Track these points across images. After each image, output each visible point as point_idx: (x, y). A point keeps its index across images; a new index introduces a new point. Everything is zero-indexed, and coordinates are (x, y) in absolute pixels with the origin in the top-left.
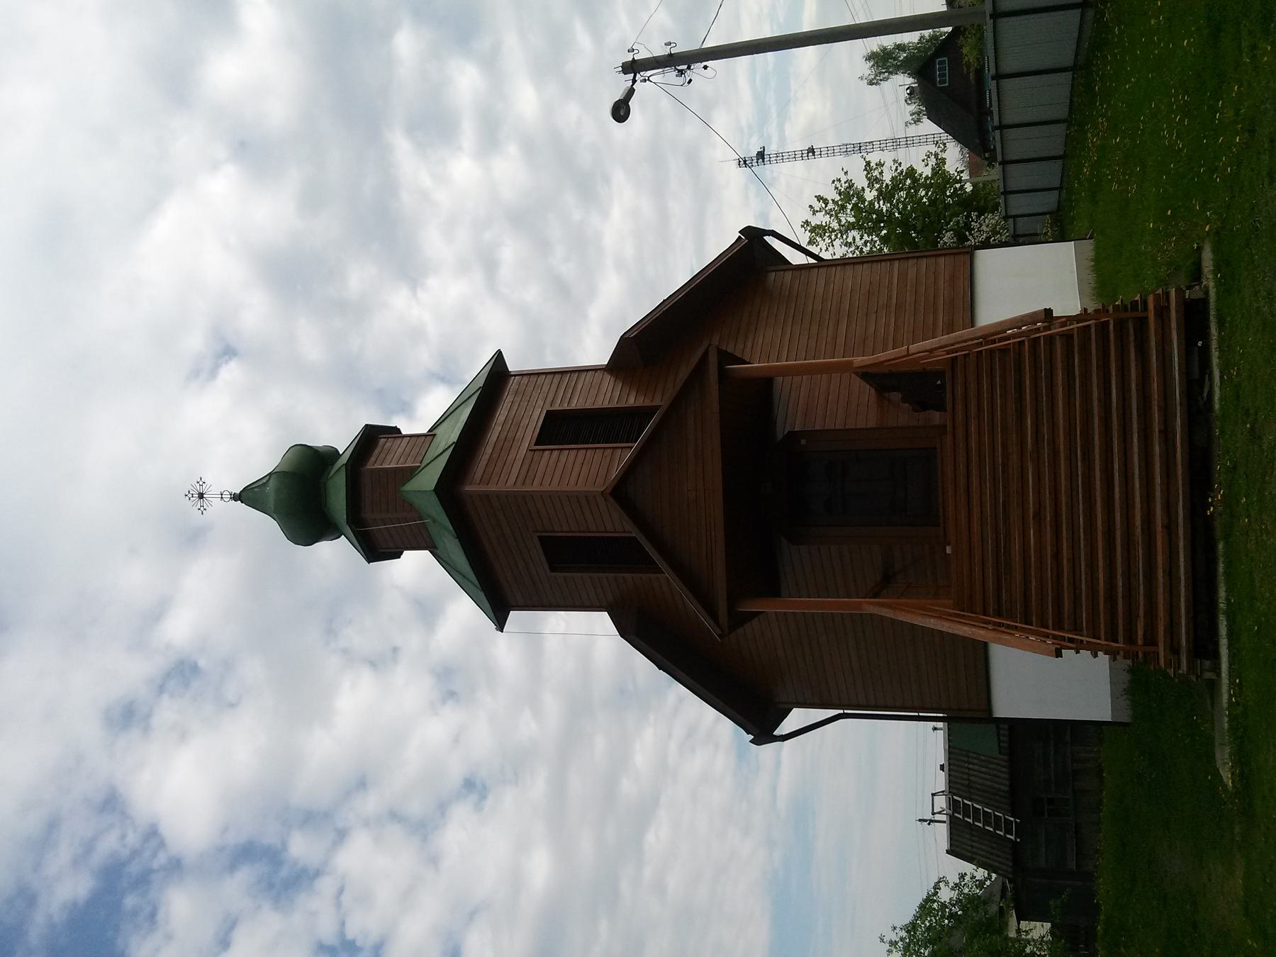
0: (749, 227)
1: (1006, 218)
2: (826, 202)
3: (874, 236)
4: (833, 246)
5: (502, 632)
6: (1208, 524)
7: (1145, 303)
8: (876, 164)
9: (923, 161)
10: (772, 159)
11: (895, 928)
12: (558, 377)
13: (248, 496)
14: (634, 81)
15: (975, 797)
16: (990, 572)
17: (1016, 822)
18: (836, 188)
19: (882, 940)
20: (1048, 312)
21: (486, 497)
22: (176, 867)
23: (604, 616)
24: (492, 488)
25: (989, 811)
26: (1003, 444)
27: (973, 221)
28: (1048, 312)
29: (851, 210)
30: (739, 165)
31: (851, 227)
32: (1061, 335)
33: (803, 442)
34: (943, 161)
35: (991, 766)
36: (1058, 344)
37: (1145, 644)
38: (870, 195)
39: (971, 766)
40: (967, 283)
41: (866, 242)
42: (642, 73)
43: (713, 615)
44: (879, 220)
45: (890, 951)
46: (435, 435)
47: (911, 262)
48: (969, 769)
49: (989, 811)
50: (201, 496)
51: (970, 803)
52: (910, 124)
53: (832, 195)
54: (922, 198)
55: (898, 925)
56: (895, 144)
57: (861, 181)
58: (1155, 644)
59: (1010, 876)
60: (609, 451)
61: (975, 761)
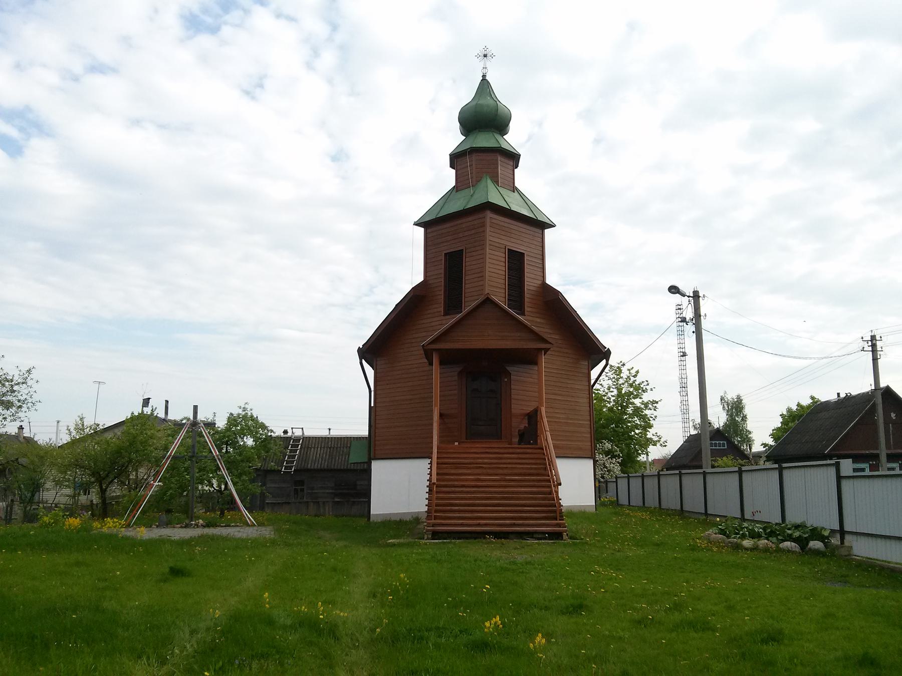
0: (610, 353)
1: (616, 478)
2: (635, 376)
3: (613, 403)
4: (609, 379)
5: (414, 225)
7: (563, 520)
8: (655, 407)
9: (656, 433)
10: (680, 327)
12: (541, 257)
13: (484, 86)
14: (689, 297)
15: (302, 451)
16: (452, 461)
17: (291, 472)
18: (643, 382)
19: (246, 403)
20: (560, 484)
21: (483, 225)
23: (422, 279)
24: (488, 229)
25: (296, 458)
26: (507, 467)
27: (616, 459)
28: (560, 484)
29: (629, 390)
30: (678, 305)
31: (619, 390)
32: (551, 491)
33: (506, 380)
34: (655, 445)
35: (320, 459)
36: (548, 489)
37: (435, 516)
38: (637, 402)
39: (319, 449)
40: (398, 457)
41: (610, 398)
42: (692, 301)
43: (433, 342)
44: (622, 406)
45: (240, 407)
46: (514, 192)
47: (589, 430)
48: (318, 448)
49: (296, 458)
50: (485, 56)
51: (299, 448)
52: (694, 422)
53: (639, 380)
54: (634, 432)
56: (685, 411)
57: (646, 397)
59: (262, 468)
60: (504, 287)
61: (322, 451)
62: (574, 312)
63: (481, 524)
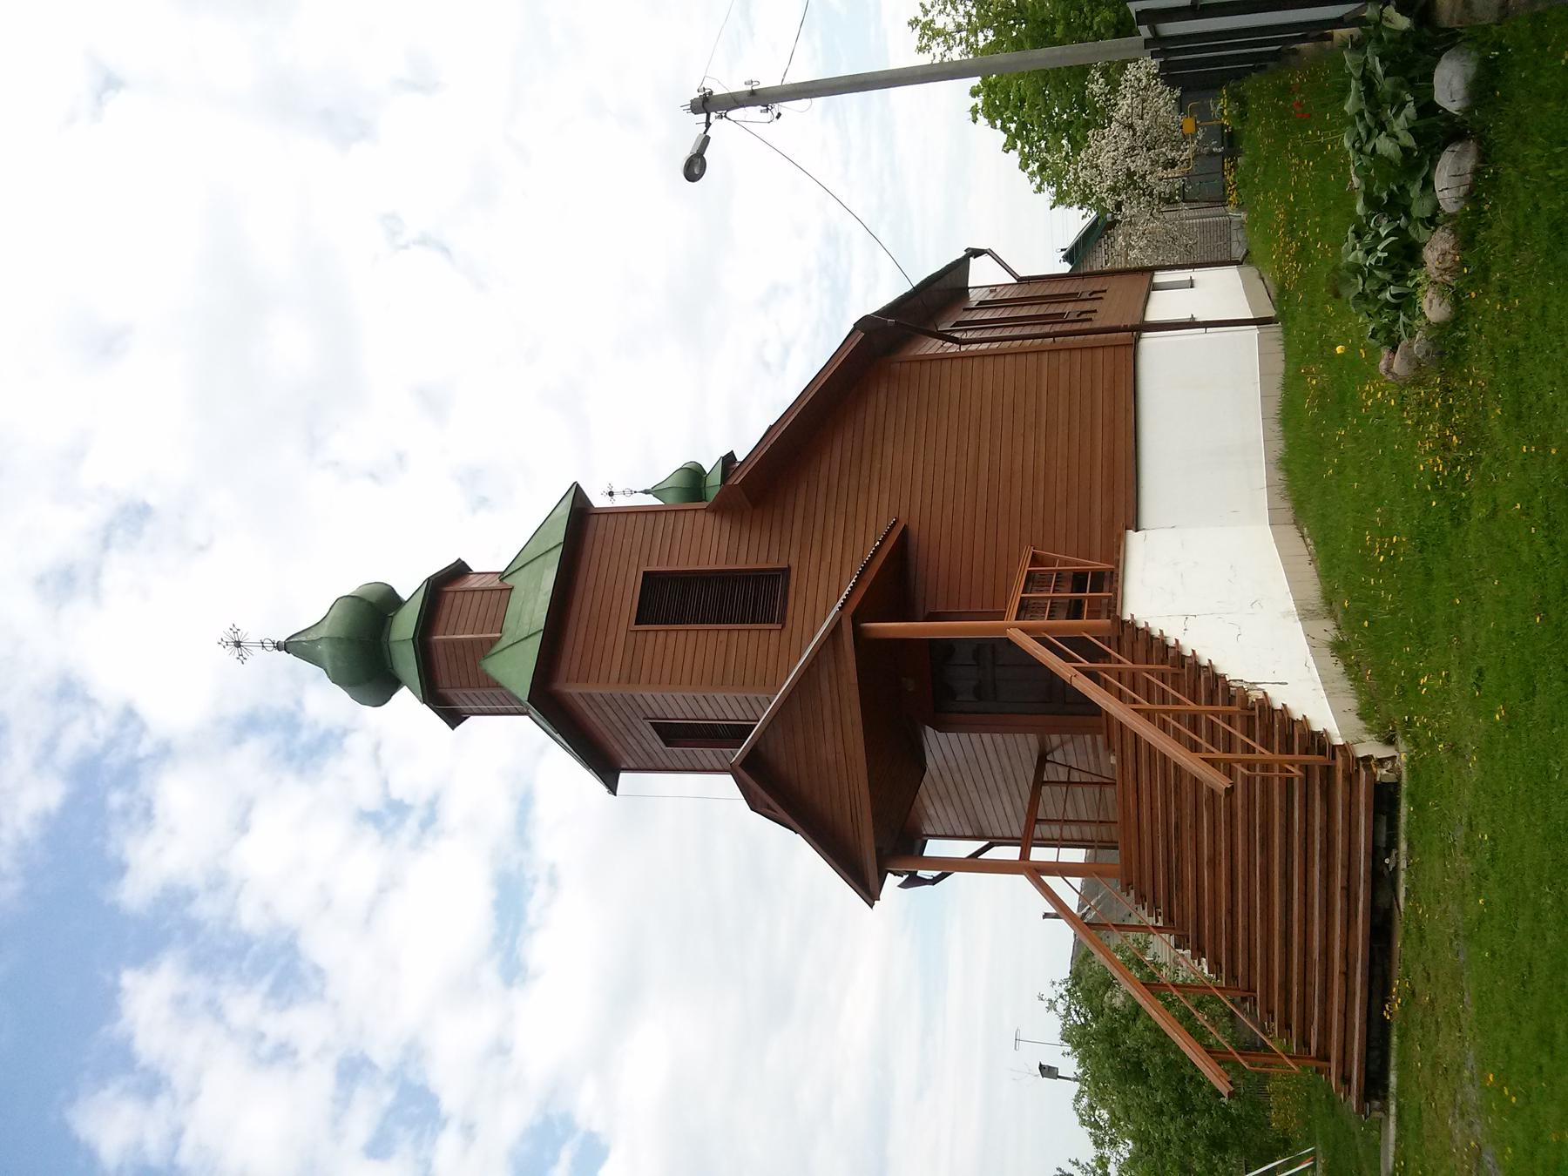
6: (1385, 1026)
11: (1054, 983)
14: (708, 125)
22: (166, 751)
46: (511, 589)
55: (1058, 981)
58: (1328, 1059)
62: (774, 430)
63: (1344, 969)
